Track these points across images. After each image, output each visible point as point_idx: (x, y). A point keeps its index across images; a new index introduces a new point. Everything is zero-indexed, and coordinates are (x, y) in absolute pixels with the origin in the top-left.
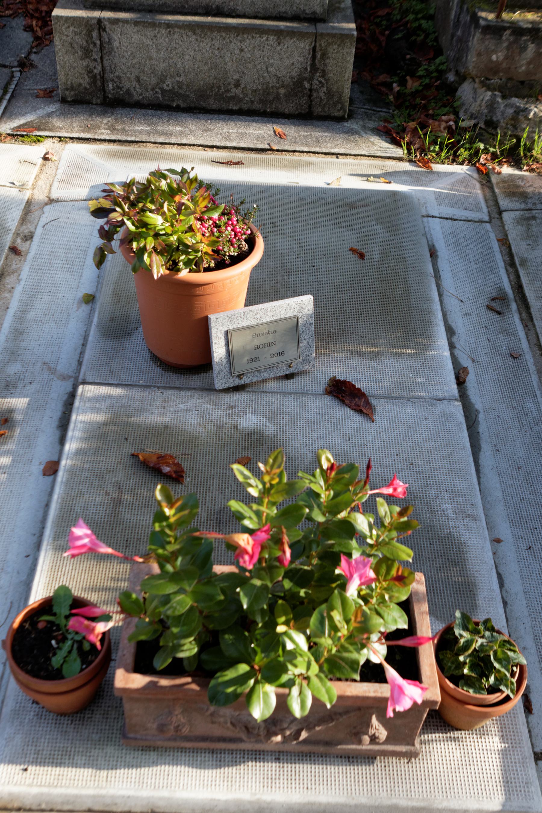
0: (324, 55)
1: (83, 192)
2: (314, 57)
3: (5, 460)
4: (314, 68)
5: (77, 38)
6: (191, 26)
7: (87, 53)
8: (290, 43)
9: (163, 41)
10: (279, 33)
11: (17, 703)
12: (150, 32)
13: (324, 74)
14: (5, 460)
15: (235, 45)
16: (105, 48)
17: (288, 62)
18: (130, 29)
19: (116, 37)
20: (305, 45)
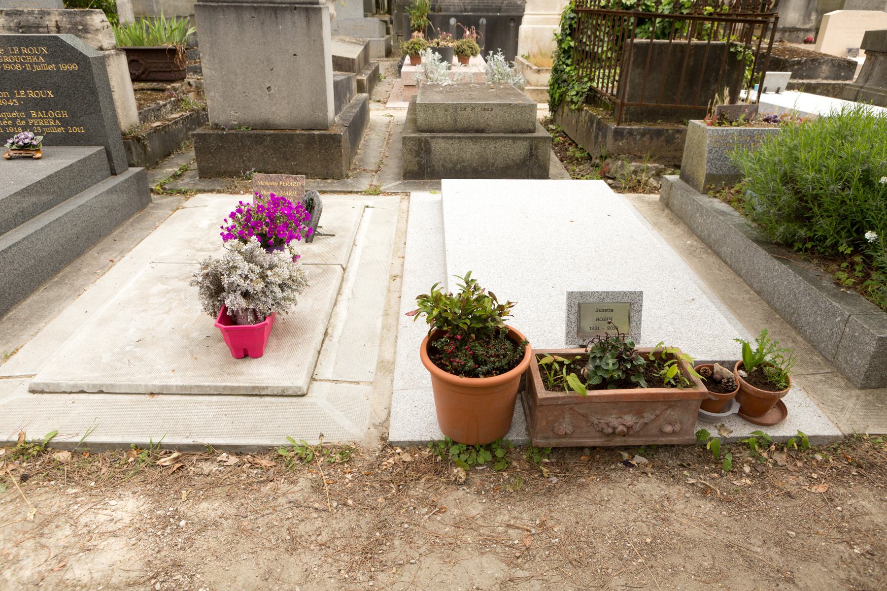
0: (537, 148)
1: (199, 313)
2: (531, 149)
3: (884, 180)
4: (532, 155)
5: (414, 147)
6: (443, 138)
7: (418, 154)
8: (519, 143)
9: (456, 145)
10: (514, 139)
11: (874, 405)
12: (450, 142)
13: (537, 157)
14: (884, 180)
15: (492, 146)
16: (428, 151)
17: (519, 152)
18: (440, 141)
19: (433, 145)
20: (526, 143)
